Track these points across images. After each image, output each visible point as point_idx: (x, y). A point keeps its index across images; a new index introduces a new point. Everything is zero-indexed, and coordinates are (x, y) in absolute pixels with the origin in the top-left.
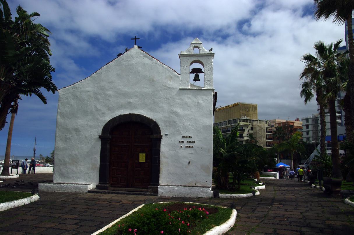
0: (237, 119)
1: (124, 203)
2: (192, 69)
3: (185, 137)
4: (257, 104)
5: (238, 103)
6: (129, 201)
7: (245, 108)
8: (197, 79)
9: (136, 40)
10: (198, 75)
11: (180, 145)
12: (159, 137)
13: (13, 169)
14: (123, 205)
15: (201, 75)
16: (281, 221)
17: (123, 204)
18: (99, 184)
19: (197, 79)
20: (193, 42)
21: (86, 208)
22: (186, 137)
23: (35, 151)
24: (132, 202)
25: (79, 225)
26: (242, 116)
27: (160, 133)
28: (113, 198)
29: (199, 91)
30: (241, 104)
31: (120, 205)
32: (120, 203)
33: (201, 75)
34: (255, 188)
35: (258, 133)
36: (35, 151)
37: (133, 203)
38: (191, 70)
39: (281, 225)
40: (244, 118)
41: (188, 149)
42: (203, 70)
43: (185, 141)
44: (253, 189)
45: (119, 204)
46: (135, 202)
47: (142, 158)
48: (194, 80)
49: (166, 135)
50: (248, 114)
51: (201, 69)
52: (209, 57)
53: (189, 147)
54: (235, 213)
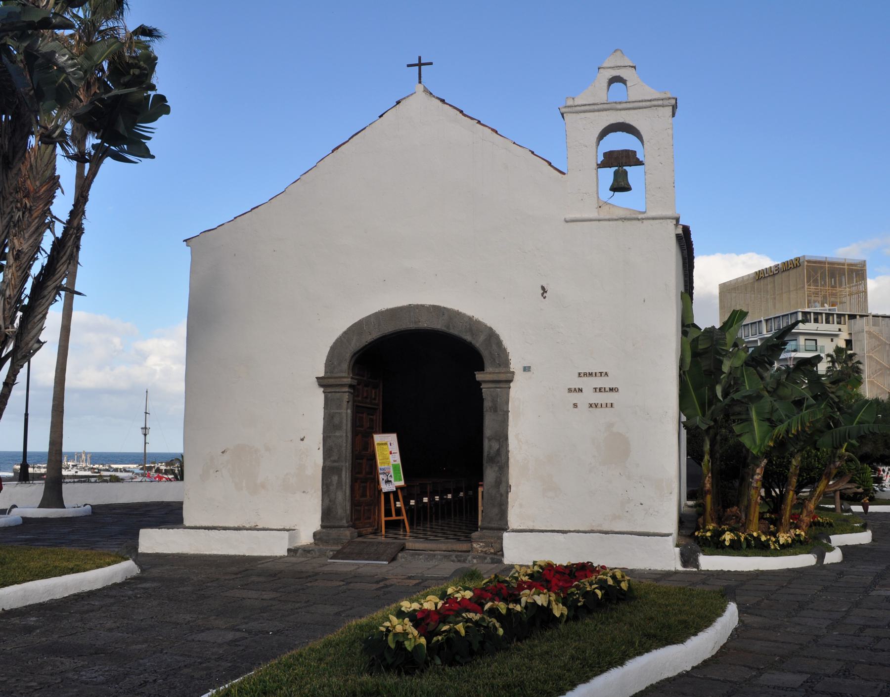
0: (796, 313)
1: (392, 585)
2: (605, 154)
3: (585, 374)
4: (865, 261)
5: (798, 259)
6: (410, 578)
7: (823, 274)
8: (620, 186)
9: (422, 67)
10: (626, 173)
11: (575, 397)
12: (502, 377)
13: (187, 523)
14: (386, 590)
15: (633, 173)
16: (878, 639)
17: (386, 586)
18: (322, 527)
19: (620, 186)
20: (605, 65)
21: (274, 599)
22: (591, 374)
23: (145, 435)
24: (417, 581)
25: (111, 597)
26: (815, 302)
27: (506, 363)
28: (360, 570)
29: (629, 222)
30: (808, 262)
31: (377, 589)
32: (379, 586)
33: (633, 173)
34: (830, 541)
35: (870, 357)
36: (145, 435)
37: (420, 583)
38: (601, 158)
39: (875, 650)
40: (818, 309)
41: (598, 410)
42: (639, 156)
43: (589, 384)
44: (825, 542)
45: (375, 586)
46: (426, 580)
47: (412, 502)
48: (614, 189)
49: (527, 369)
50: (834, 295)
51: (635, 152)
52: (660, 108)
53: (604, 405)
54: (732, 609)
